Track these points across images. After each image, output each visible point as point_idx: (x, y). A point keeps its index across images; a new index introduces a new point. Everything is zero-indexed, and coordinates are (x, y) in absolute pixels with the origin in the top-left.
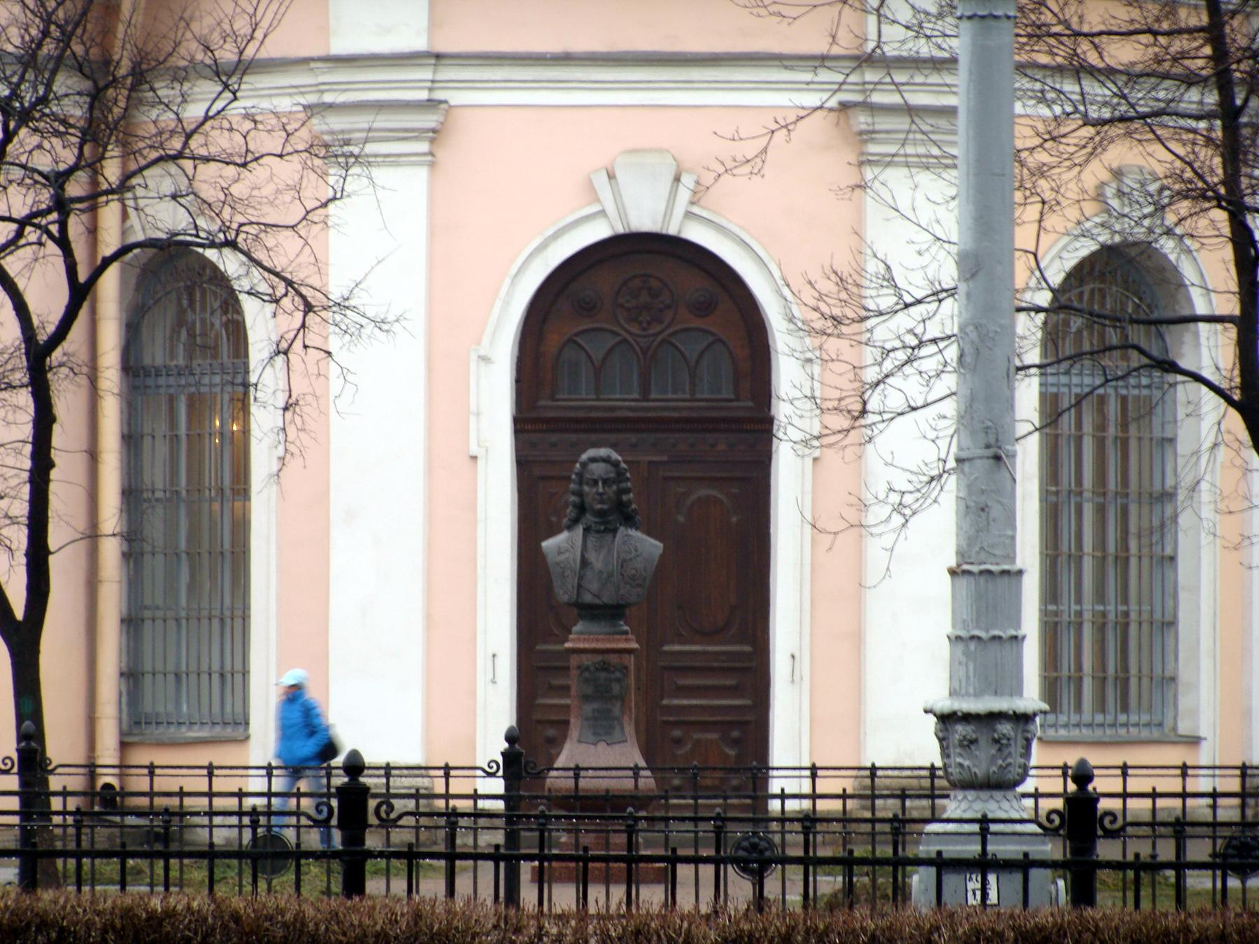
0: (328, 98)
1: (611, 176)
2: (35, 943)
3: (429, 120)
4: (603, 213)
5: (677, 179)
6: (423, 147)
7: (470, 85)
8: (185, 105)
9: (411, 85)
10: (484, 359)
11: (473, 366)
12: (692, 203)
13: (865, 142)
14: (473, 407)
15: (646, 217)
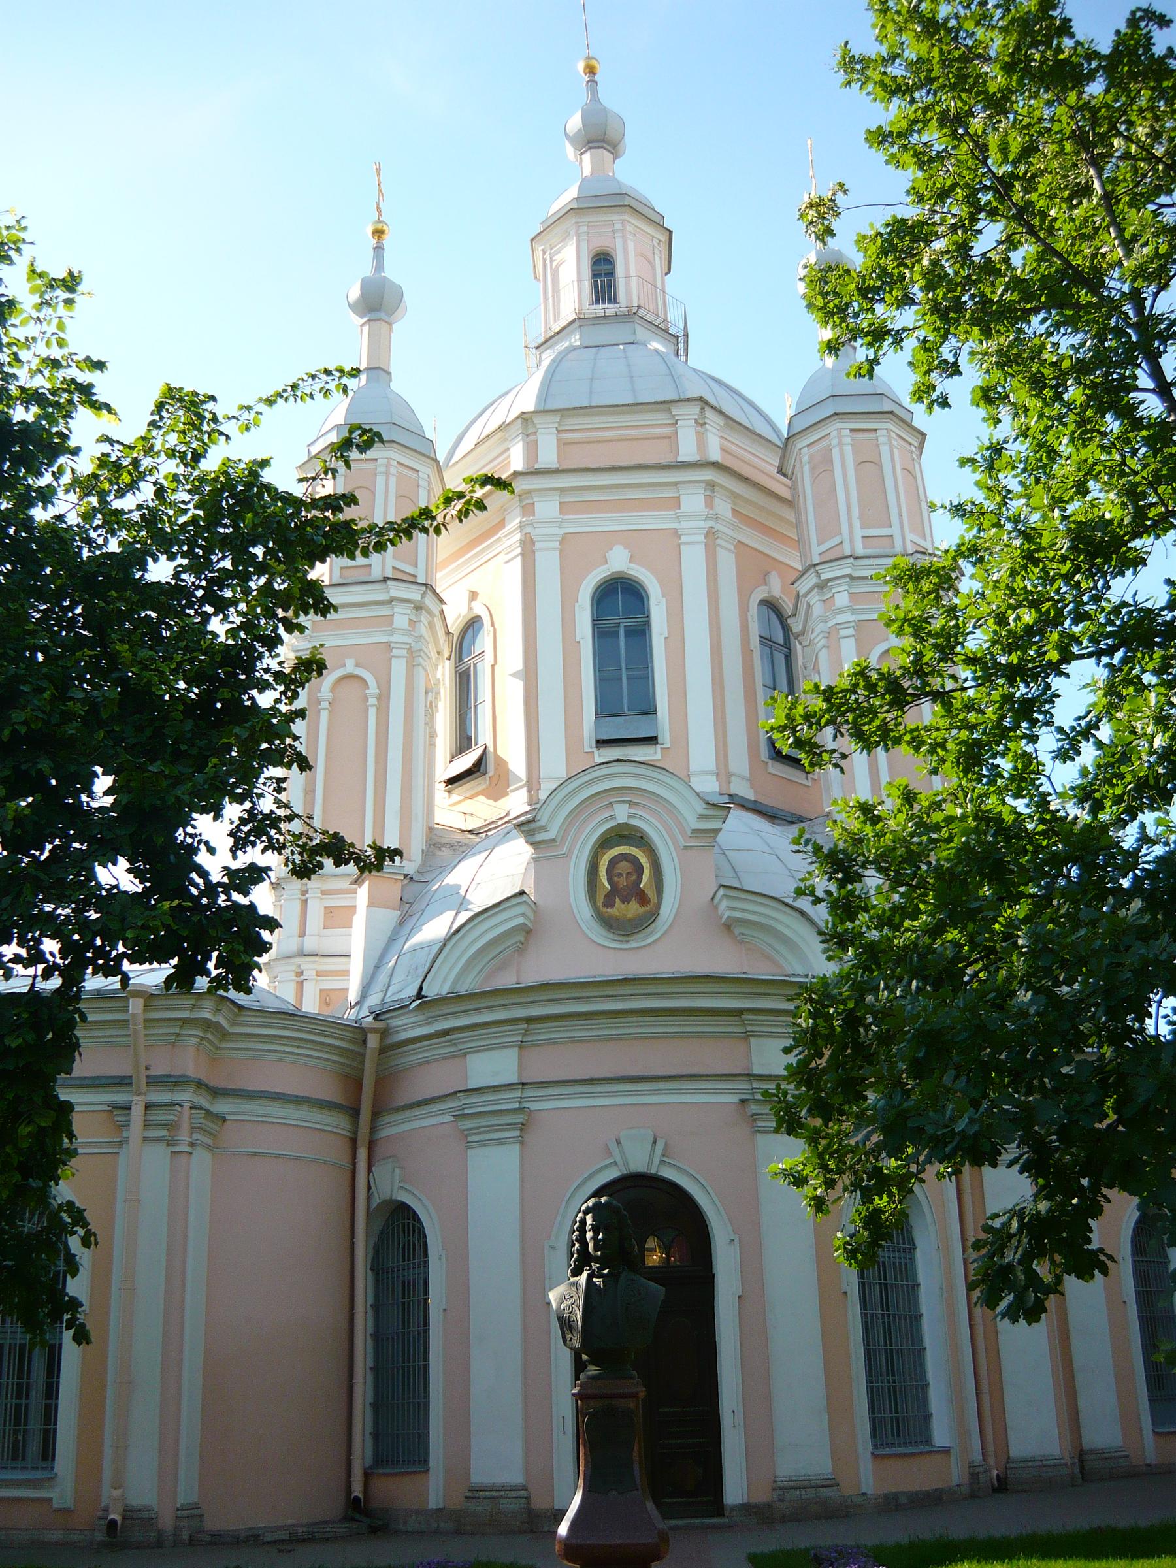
0: (466, 1111)
1: (618, 1142)
2: (1175, 129)
3: (519, 1118)
4: (615, 1163)
5: (655, 1143)
6: (517, 1133)
7: (542, 1098)
8: (881, 94)
9: (510, 1099)
10: (553, 1248)
11: (546, 1252)
12: (663, 1155)
13: (756, 1120)
14: (547, 1275)
15: (639, 1162)
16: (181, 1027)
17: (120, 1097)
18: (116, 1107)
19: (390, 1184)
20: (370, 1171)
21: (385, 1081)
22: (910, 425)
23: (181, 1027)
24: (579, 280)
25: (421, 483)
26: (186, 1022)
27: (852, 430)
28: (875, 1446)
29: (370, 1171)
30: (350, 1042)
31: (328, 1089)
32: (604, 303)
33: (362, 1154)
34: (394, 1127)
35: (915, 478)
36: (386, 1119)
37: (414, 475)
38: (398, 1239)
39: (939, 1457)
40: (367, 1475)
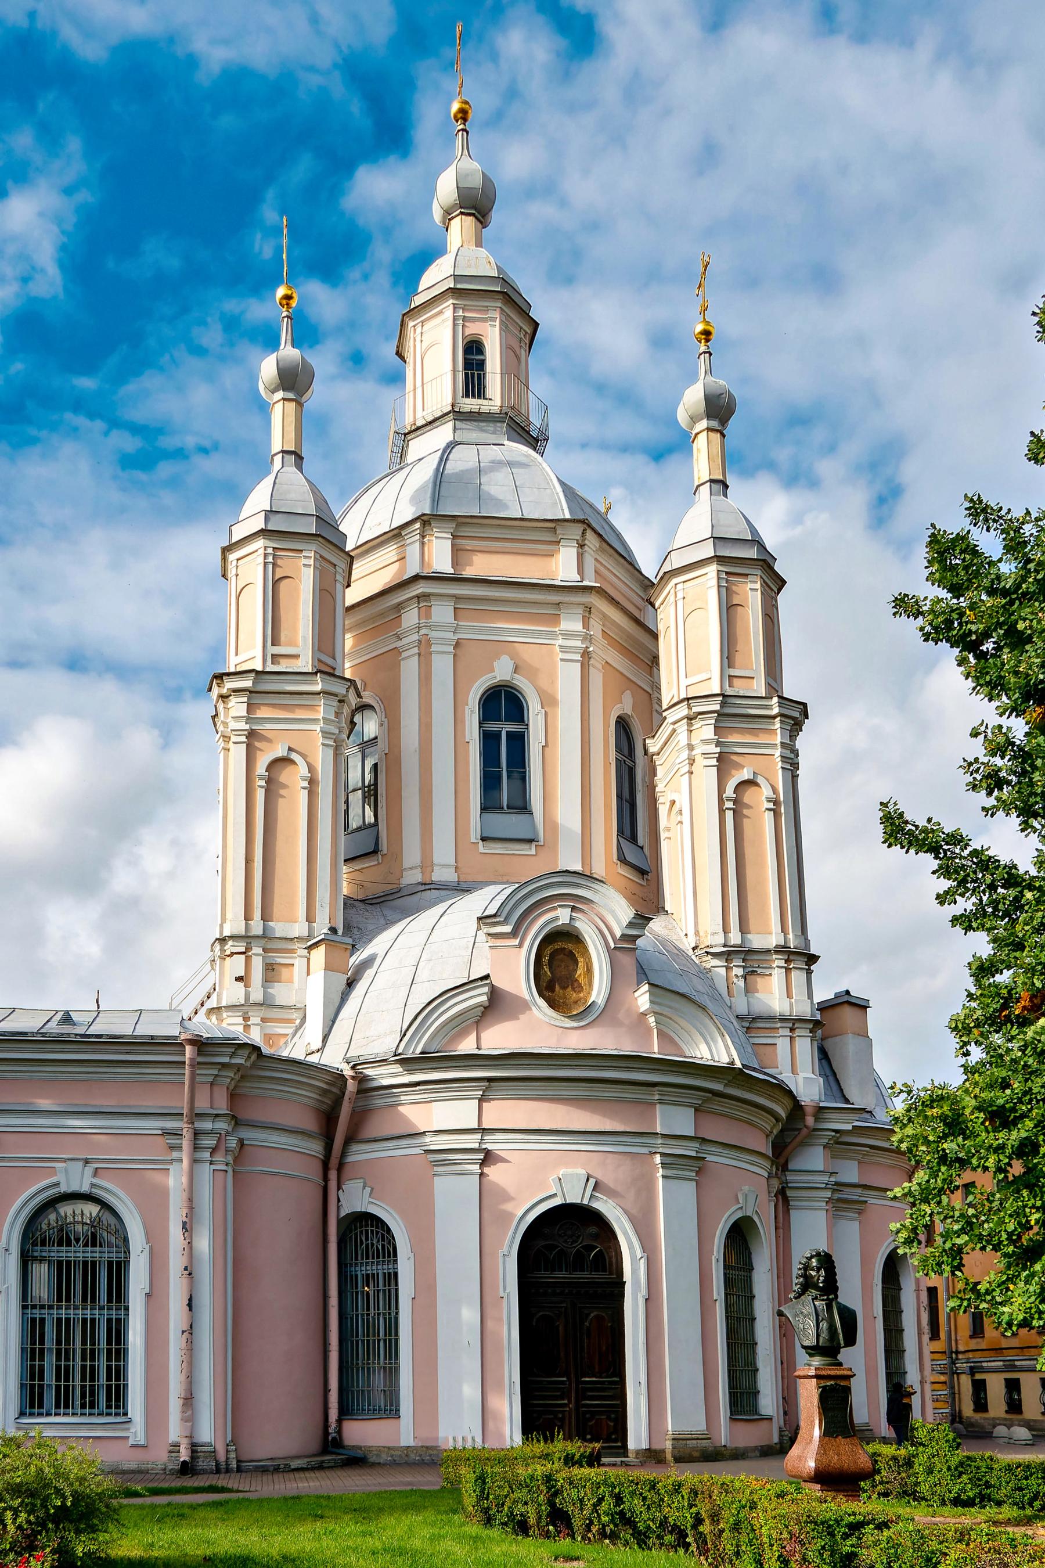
5: (588, 1180)
16: (220, 1070)
17: (171, 1124)
18: (166, 1133)
19: (355, 1198)
20: (339, 1188)
21: (360, 1117)
22: (772, 569)
23: (220, 1070)
24: (454, 371)
25: (338, 577)
26: (224, 1066)
27: (727, 573)
28: (731, 1414)
29: (339, 1188)
30: (326, 1083)
31: (309, 1122)
32: (473, 396)
33: (333, 1175)
34: (359, 1154)
35: (519, 361)
36: (354, 1147)
37: (331, 568)
38: (364, 1240)
39: (765, 1422)
40: (340, 1421)
